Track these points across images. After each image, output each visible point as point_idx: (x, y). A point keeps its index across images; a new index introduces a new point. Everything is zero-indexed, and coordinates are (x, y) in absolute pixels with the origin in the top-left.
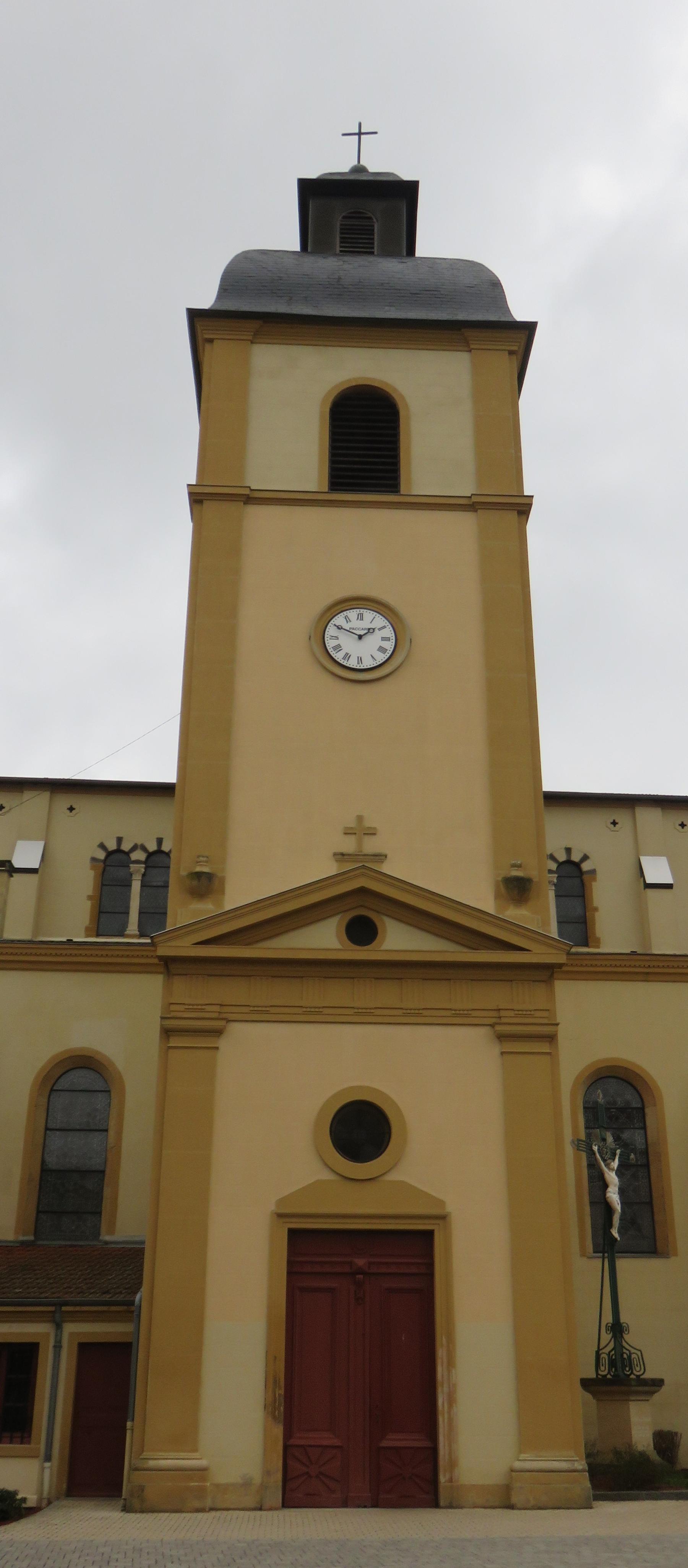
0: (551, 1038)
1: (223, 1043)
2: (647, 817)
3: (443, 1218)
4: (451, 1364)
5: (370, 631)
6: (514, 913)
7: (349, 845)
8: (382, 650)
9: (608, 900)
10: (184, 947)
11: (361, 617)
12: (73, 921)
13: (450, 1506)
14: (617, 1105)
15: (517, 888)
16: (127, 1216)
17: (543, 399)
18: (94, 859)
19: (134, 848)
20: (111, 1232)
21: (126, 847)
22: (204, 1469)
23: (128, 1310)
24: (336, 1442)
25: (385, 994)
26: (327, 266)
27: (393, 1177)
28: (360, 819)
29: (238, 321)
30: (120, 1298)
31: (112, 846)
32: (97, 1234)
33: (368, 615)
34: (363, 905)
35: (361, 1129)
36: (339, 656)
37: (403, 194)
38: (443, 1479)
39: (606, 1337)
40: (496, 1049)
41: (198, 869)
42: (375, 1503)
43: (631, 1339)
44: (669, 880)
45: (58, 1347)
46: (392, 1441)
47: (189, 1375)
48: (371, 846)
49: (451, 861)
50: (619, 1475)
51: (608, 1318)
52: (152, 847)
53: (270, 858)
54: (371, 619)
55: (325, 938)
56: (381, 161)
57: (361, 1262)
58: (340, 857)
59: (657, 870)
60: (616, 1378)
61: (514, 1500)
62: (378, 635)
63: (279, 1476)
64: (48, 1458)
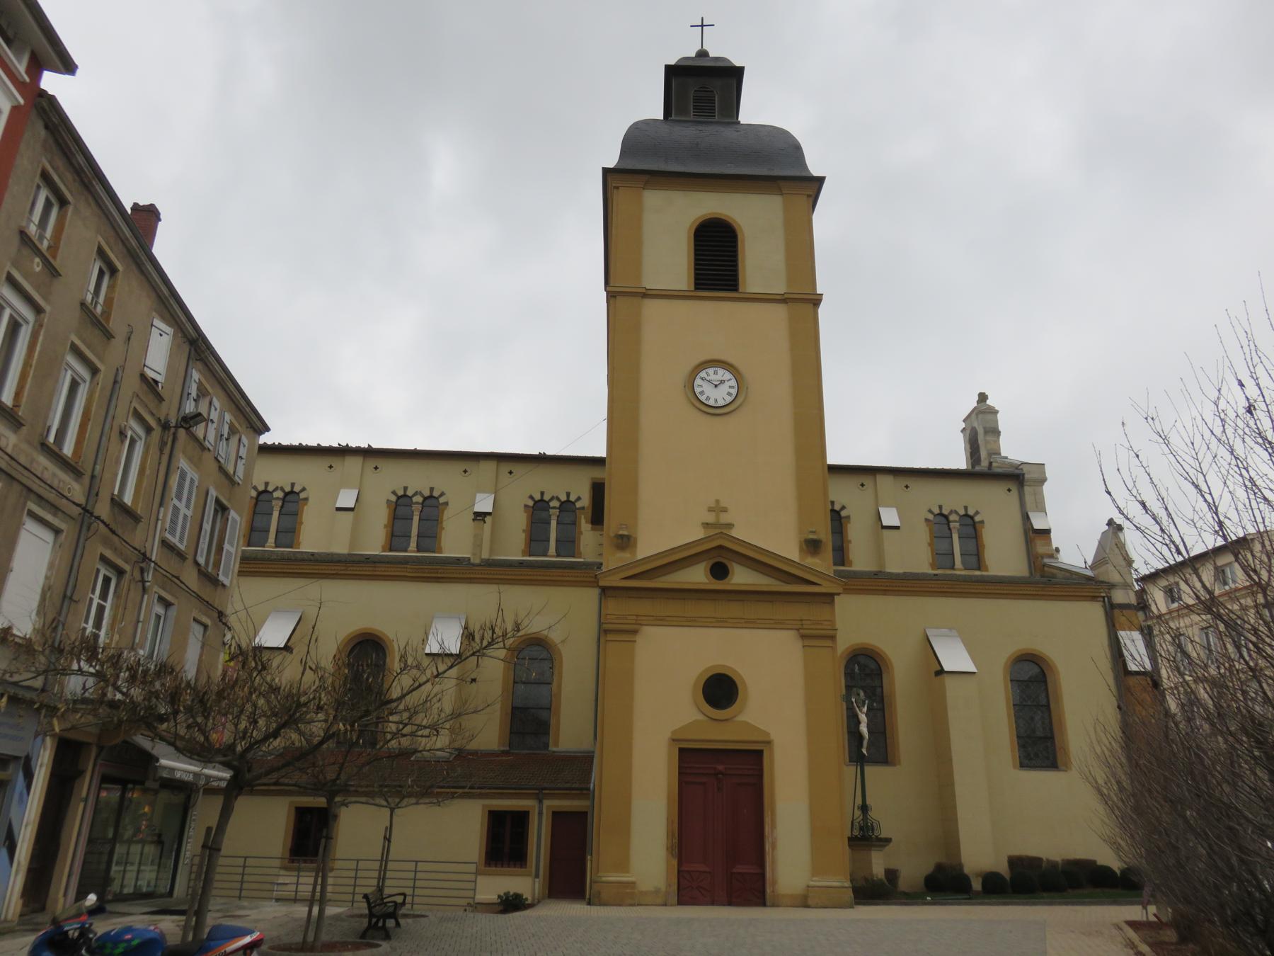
0: (833, 638)
1: (639, 638)
2: (885, 482)
3: (769, 743)
4: (773, 826)
5: (722, 382)
6: (811, 561)
7: (711, 518)
8: (729, 394)
9: (857, 534)
10: (614, 581)
11: (716, 373)
12: (513, 548)
13: (773, 905)
14: (865, 672)
15: (812, 546)
16: (569, 734)
17: (827, 221)
18: (526, 506)
19: (552, 498)
20: (556, 744)
21: (546, 498)
22: (634, 883)
23: (584, 790)
24: (707, 869)
25: (735, 609)
26: (686, 133)
27: (740, 718)
28: (717, 501)
29: (636, 173)
30: (576, 786)
31: (538, 497)
32: (546, 746)
33: (721, 371)
34: (720, 556)
35: (720, 690)
36: (703, 398)
37: (735, 74)
38: (768, 891)
39: (858, 813)
40: (799, 644)
41: (621, 532)
42: (730, 904)
43: (873, 814)
44: (897, 523)
45: (540, 813)
46: (740, 869)
47: (623, 829)
48: (725, 518)
49: (774, 530)
50: (872, 891)
51: (859, 801)
52: (563, 498)
53: (664, 523)
54: (723, 374)
55: (698, 576)
56: (721, 48)
57: (721, 767)
58: (706, 525)
59: (890, 517)
60: (864, 837)
61: (810, 902)
62: (727, 384)
63: (676, 887)
64: (537, 876)
